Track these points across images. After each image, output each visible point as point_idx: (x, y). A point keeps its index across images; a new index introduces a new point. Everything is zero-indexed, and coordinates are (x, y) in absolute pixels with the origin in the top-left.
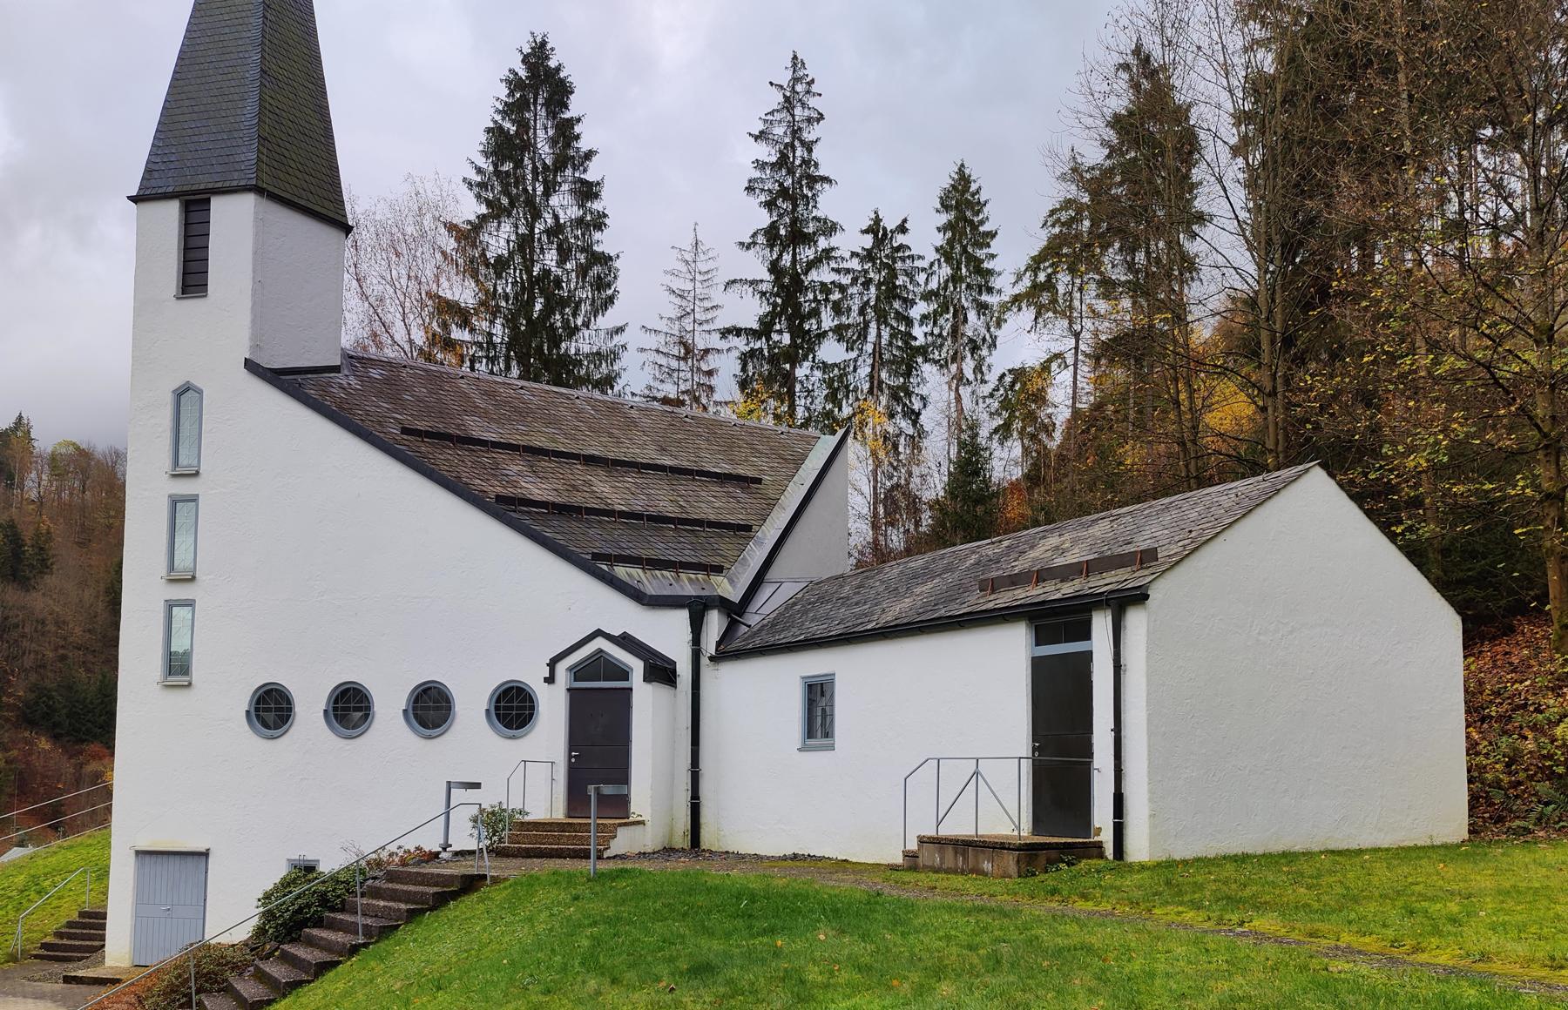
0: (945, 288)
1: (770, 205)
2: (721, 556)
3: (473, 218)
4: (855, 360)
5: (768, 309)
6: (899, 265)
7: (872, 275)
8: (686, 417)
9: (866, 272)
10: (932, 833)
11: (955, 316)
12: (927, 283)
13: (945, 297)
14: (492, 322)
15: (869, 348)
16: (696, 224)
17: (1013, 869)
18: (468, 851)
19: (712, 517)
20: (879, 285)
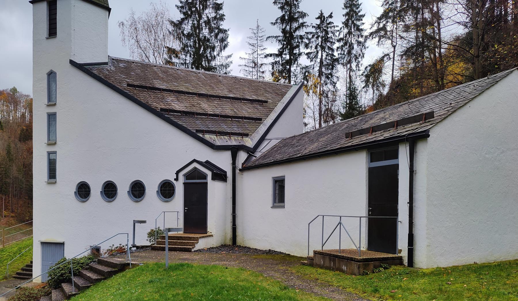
0: (346, 37)
1: (282, 8)
2: (248, 130)
3: (179, 19)
4: (314, 65)
5: (281, 46)
6: (329, 29)
7: (319, 34)
8: (241, 79)
9: (317, 33)
10: (319, 248)
11: (349, 47)
12: (339, 35)
13: (345, 40)
14: (186, 56)
15: (318, 60)
16: (258, 20)
17: (356, 270)
18: (146, 246)
19: (247, 116)
20: (322, 37)
